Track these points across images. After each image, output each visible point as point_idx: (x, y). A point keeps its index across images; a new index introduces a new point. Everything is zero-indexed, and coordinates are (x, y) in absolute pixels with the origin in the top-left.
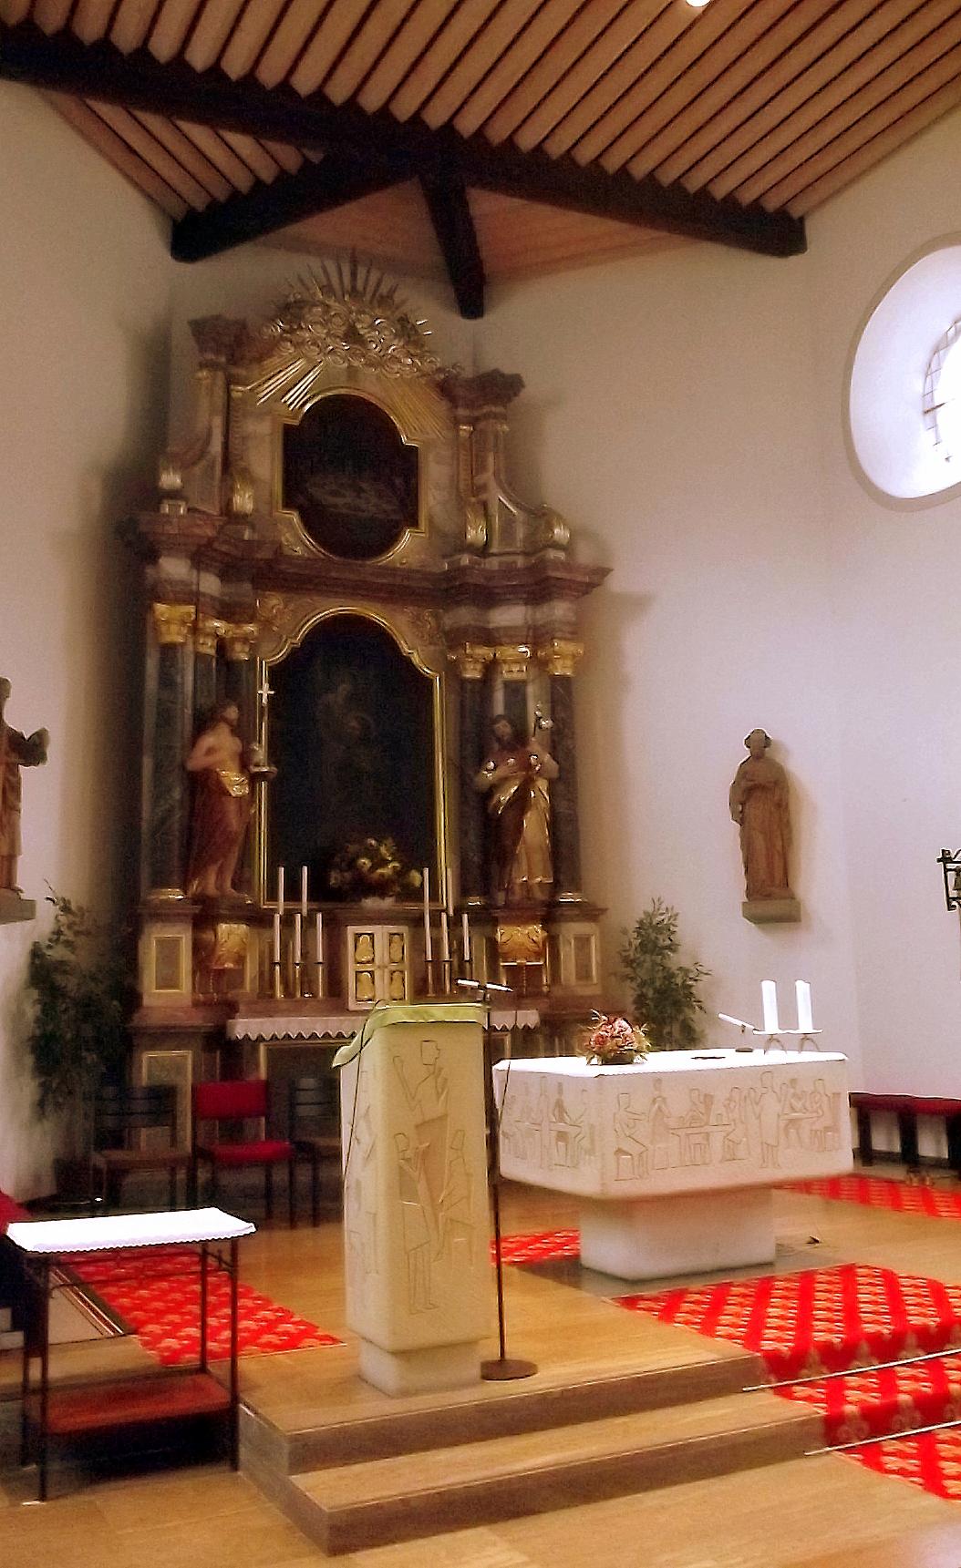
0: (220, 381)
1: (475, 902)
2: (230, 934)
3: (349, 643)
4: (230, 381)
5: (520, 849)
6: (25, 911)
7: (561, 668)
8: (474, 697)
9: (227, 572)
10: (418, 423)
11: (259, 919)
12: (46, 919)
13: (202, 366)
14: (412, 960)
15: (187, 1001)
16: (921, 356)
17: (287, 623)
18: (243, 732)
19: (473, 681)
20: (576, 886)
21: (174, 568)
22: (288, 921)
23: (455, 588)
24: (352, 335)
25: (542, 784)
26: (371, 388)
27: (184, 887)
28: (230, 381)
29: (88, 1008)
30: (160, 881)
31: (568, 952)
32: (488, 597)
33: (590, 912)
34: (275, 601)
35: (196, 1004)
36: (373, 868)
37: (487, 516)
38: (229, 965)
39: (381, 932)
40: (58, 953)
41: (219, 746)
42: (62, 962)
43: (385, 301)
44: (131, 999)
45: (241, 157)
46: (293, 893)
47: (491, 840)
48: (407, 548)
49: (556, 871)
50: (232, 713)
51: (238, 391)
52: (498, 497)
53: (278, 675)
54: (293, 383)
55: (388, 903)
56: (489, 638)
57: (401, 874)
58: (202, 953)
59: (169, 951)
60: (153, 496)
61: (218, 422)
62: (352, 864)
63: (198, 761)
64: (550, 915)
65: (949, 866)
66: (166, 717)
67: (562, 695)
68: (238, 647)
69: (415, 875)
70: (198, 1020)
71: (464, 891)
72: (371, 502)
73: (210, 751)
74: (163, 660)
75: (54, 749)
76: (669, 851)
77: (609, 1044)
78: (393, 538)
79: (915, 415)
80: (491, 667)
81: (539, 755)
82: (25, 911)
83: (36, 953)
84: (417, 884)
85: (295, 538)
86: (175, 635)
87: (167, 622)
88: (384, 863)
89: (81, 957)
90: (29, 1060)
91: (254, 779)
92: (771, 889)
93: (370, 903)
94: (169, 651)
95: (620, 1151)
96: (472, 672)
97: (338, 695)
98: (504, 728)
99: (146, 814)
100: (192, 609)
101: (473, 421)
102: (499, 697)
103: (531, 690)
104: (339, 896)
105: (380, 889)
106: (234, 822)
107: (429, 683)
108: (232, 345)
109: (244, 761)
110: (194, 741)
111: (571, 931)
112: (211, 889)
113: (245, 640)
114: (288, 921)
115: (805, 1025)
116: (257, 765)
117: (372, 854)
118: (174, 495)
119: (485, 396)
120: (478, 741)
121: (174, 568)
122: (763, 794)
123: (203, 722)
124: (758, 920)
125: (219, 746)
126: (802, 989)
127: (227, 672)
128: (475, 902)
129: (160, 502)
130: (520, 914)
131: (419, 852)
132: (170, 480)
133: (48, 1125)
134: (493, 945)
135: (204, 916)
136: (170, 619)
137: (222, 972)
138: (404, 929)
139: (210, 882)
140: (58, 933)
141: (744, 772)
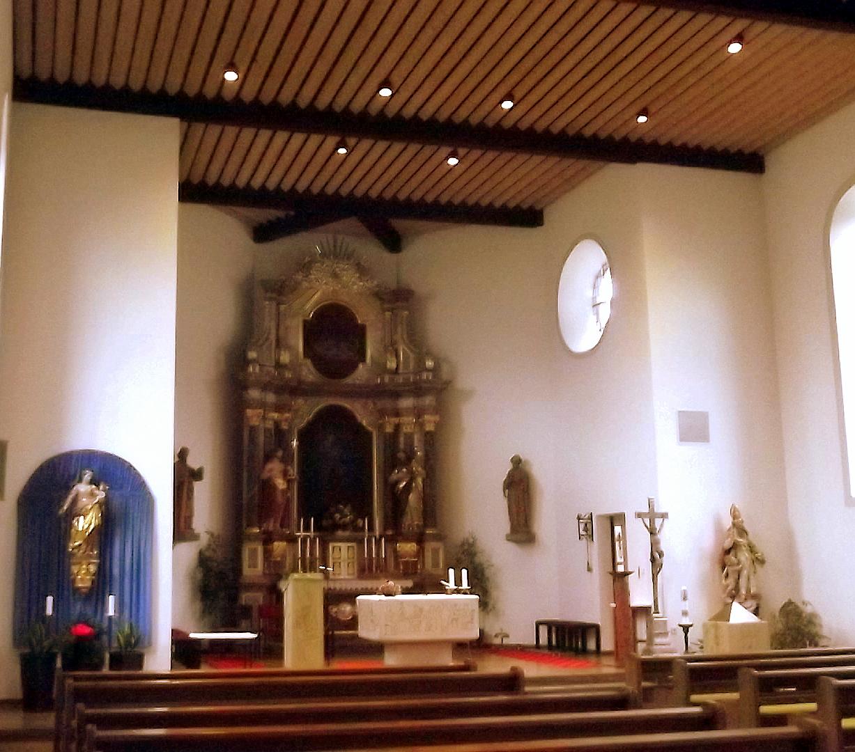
0: (274, 304)
1: (390, 532)
2: (279, 546)
3: (336, 419)
4: (278, 304)
5: (408, 510)
6: (195, 537)
7: (430, 427)
8: (391, 441)
9: (279, 390)
10: (367, 315)
11: (292, 540)
12: (204, 540)
13: (266, 299)
14: (358, 558)
15: (261, 573)
16: (591, 279)
17: (306, 410)
18: (286, 460)
19: (390, 434)
20: (434, 526)
21: (254, 394)
22: (304, 541)
23: (383, 393)
24: (335, 276)
25: (420, 480)
26: (344, 299)
27: (260, 528)
28: (278, 304)
29: (221, 575)
30: (250, 525)
31: (428, 555)
32: (396, 395)
33: (439, 538)
34: (300, 401)
35: (264, 574)
36: (340, 518)
37: (397, 356)
38: (279, 559)
39: (344, 546)
40: (207, 554)
41: (274, 469)
42: (210, 557)
43: (349, 257)
44: (238, 570)
45: (271, 214)
46: (307, 528)
47: (396, 503)
48: (361, 374)
49: (425, 519)
50: (280, 453)
51: (282, 307)
52: (402, 349)
53: (305, 436)
54: (310, 301)
55: (347, 534)
56: (397, 414)
57: (353, 521)
58: (268, 554)
59: (254, 552)
60: (246, 362)
61: (273, 324)
62: (332, 517)
63: (265, 475)
64: (420, 540)
65: (581, 521)
66: (252, 457)
67: (431, 440)
68: (283, 424)
69: (360, 522)
70: (265, 581)
71: (385, 528)
72: (343, 352)
73: (271, 470)
74: (251, 431)
75: (207, 475)
76: (480, 512)
77: (385, 590)
78: (354, 367)
79: (589, 308)
80: (397, 427)
81: (417, 467)
82: (195, 537)
83: (201, 553)
84: (361, 524)
85: (309, 373)
86: (255, 422)
87: (252, 417)
88: (347, 516)
89: (219, 555)
90: (199, 595)
91: (289, 482)
92: (522, 528)
93: (340, 533)
94: (253, 429)
95: (386, 625)
96: (389, 429)
97: (329, 443)
98: (401, 455)
99: (244, 496)
100: (261, 411)
101: (392, 310)
102: (402, 439)
103: (416, 437)
104: (327, 531)
105: (344, 527)
106: (280, 499)
107: (368, 435)
108: (279, 290)
109: (285, 474)
110: (264, 468)
111: (430, 546)
112: (271, 528)
113: (286, 420)
114: (304, 541)
115: (465, 585)
116: (290, 476)
117: (341, 512)
118: (254, 361)
119: (399, 299)
120: (392, 462)
121: (254, 394)
122: (519, 486)
123: (268, 458)
124: (517, 542)
125: (275, 467)
126: (464, 572)
127: (280, 436)
128: (390, 532)
129: (248, 366)
130: (407, 539)
131: (364, 509)
132: (252, 355)
133: (206, 620)
134: (395, 551)
135: (268, 539)
136: (253, 416)
137: (276, 562)
138: (354, 544)
139: (271, 525)
140: (209, 545)
141: (510, 475)
